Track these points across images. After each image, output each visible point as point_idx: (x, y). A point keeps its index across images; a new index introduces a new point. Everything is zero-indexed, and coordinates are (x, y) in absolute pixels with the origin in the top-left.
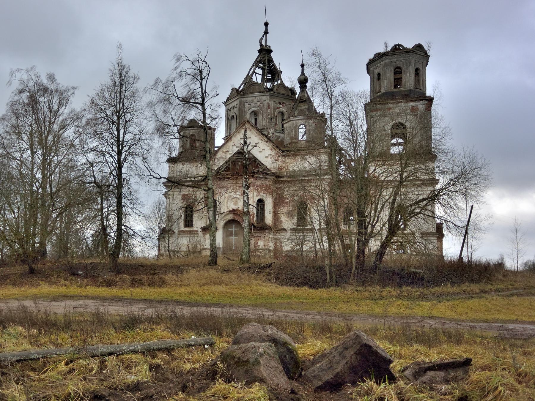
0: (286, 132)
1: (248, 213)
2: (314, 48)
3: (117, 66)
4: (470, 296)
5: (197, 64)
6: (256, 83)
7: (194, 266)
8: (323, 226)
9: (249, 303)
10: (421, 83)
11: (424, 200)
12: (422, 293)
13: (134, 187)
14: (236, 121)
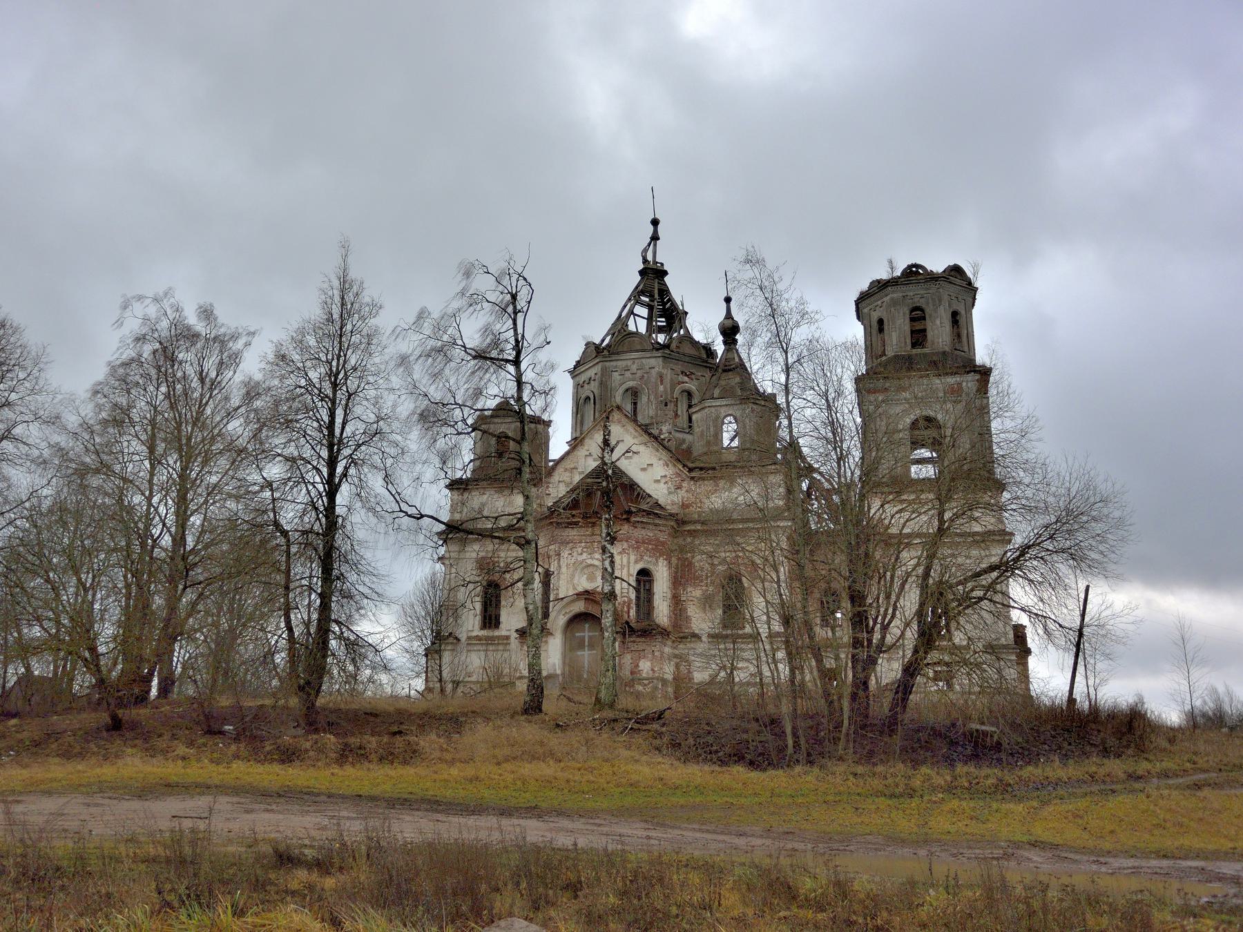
0: (697, 430)
1: (612, 595)
2: (751, 249)
3: (336, 283)
4: (1108, 787)
5: (506, 282)
6: (637, 333)
7: (486, 715)
8: (777, 627)
9: (605, 806)
10: (964, 339)
11: (992, 568)
12: (1001, 781)
13: (360, 534)
14: (593, 407)
